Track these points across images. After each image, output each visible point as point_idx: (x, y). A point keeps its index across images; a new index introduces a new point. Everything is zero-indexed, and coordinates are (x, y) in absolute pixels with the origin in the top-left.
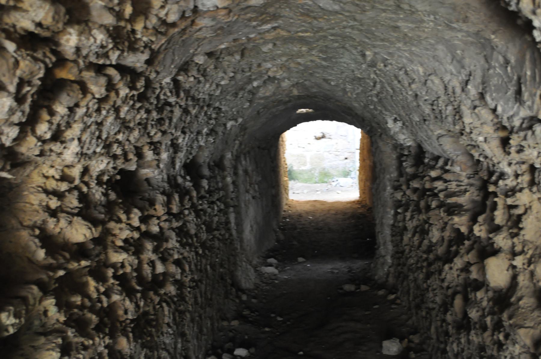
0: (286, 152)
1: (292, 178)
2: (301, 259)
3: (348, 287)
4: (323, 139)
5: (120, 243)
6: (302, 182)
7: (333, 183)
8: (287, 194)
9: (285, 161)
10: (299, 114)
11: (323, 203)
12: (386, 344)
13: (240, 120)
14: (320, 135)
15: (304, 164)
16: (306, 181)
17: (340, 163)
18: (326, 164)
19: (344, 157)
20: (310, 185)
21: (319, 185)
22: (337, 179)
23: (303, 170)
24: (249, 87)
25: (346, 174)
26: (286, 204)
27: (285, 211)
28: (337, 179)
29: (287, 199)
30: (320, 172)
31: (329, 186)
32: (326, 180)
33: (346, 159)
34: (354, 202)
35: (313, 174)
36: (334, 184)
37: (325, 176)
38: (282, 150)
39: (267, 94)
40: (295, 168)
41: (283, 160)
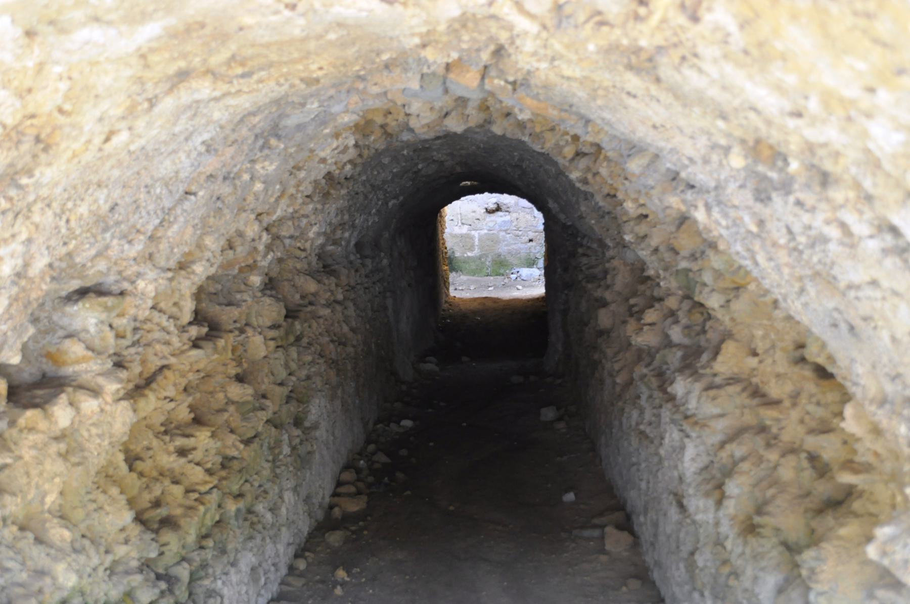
0: (446, 231)
1: (453, 269)
2: (465, 359)
3: (516, 379)
4: (500, 213)
5: (323, 302)
6: (468, 274)
7: (512, 276)
8: (448, 289)
9: (444, 244)
10: (463, 187)
11: (496, 300)
12: (544, 411)
13: (401, 198)
14: (493, 207)
15: (471, 249)
16: (473, 273)
17: (522, 247)
18: (503, 249)
19: (527, 239)
20: (479, 278)
21: (492, 278)
22: (518, 270)
23: (469, 257)
24: (415, 169)
25: (531, 263)
26: (446, 302)
27: (444, 310)
28: (518, 270)
29: (447, 295)
30: (493, 260)
31: (506, 280)
32: (502, 271)
33: (531, 240)
34: (538, 299)
35: (482, 263)
36: (513, 276)
37: (500, 266)
38: (440, 228)
39: (430, 172)
40: (457, 254)
41: (442, 242)
